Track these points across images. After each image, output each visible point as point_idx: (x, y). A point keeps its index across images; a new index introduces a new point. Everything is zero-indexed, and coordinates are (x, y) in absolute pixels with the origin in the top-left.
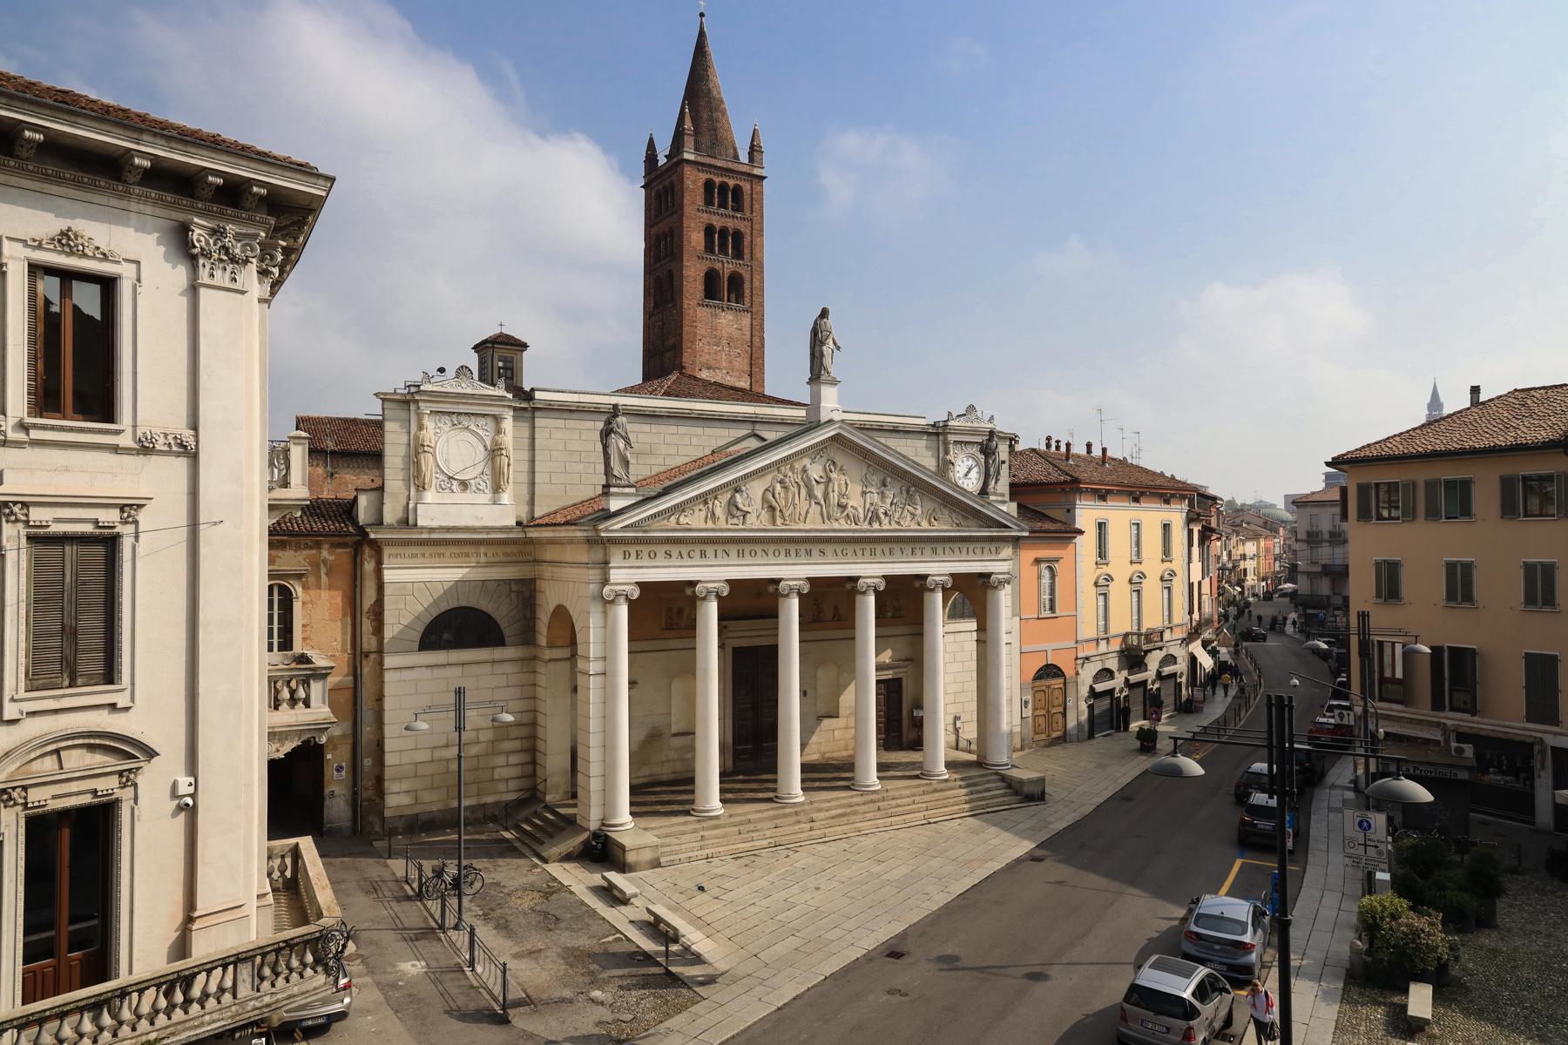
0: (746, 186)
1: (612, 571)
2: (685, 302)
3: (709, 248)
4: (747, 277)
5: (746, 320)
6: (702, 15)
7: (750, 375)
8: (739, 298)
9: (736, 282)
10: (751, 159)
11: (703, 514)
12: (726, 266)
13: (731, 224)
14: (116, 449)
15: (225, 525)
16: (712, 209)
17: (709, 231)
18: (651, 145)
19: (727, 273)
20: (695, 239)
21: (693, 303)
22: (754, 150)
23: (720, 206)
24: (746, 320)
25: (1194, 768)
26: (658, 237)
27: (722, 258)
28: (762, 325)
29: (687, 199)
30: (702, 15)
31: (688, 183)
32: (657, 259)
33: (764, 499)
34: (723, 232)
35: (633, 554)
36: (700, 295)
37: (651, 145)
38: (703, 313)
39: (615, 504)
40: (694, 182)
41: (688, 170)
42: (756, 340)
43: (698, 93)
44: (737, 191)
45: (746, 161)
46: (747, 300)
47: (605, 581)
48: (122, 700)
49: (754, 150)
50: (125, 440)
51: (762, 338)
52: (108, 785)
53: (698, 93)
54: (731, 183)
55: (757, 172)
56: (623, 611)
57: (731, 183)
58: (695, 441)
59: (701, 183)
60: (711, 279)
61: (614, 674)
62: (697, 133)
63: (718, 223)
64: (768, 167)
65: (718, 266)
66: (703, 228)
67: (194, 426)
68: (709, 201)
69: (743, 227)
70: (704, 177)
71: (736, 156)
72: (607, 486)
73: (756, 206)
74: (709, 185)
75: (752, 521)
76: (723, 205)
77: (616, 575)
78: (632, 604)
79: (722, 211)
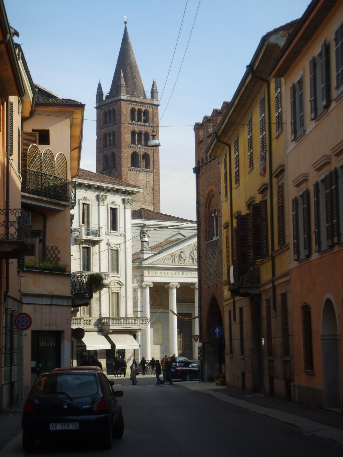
0: (150, 110)
1: (145, 278)
2: (123, 169)
3: (133, 142)
4: (151, 155)
5: (151, 176)
6: (126, 23)
7: (154, 204)
8: (147, 165)
9: (146, 157)
10: (152, 96)
11: (171, 260)
12: (141, 150)
13: (143, 129)
14: (118, 236)
15: (129, 249)
16: (134, 122)
17: (133, 133)
18: (100, 87)
19: (142, 153)
20: (127, 137)
21: (126, 169)
22: (154, 92)
23: (138, 121)
24: (151, 176)
25: (119, 84)
26: (105, 135)
27: (140, 146)
28: (159, 179)
29: (123, 118)
30: (126, 23)
31: (124, 110)
32: (105, 145)
33: (190, 255)
34: (140, 133)
35: (151, 273)
36: (129, 165)
37: (100, 87)
38: (131, 174)
39: (145, 256)
40: (126, 110)
41: (123, 103)
42: (156, 187)
43: (125, 64)
44: (146, 113)
45: (150, 97)
46: (151, 167)
47: (142, 281)
48: (119, 276)
49: (154, 92)
50: (119, 234)
51: (159, 186)
52: (118, 289)
53: (125, 64)
54: (143, 109)
55: (155, 103)
56: (148, 291)
57: (143, 109)
58: (159, 236)
59: (129, 110)
60: (134, 157)
61: (146, 311)
62: (127, 86)
63: (137, 129)
64: (162, 100)
65: (137, 150)
66: (130, 132)
67: (125, 232)
68: (133, 119)
69: (150, 130)
70: (130, 107)
71: (145, 96)
72: (142, 250)
73: (155, 120)
74: (133, 111)
75: (186, 262)
76: (139, 120)
77: (146, 279)
78: (151, 289)
79: (139, 123)
